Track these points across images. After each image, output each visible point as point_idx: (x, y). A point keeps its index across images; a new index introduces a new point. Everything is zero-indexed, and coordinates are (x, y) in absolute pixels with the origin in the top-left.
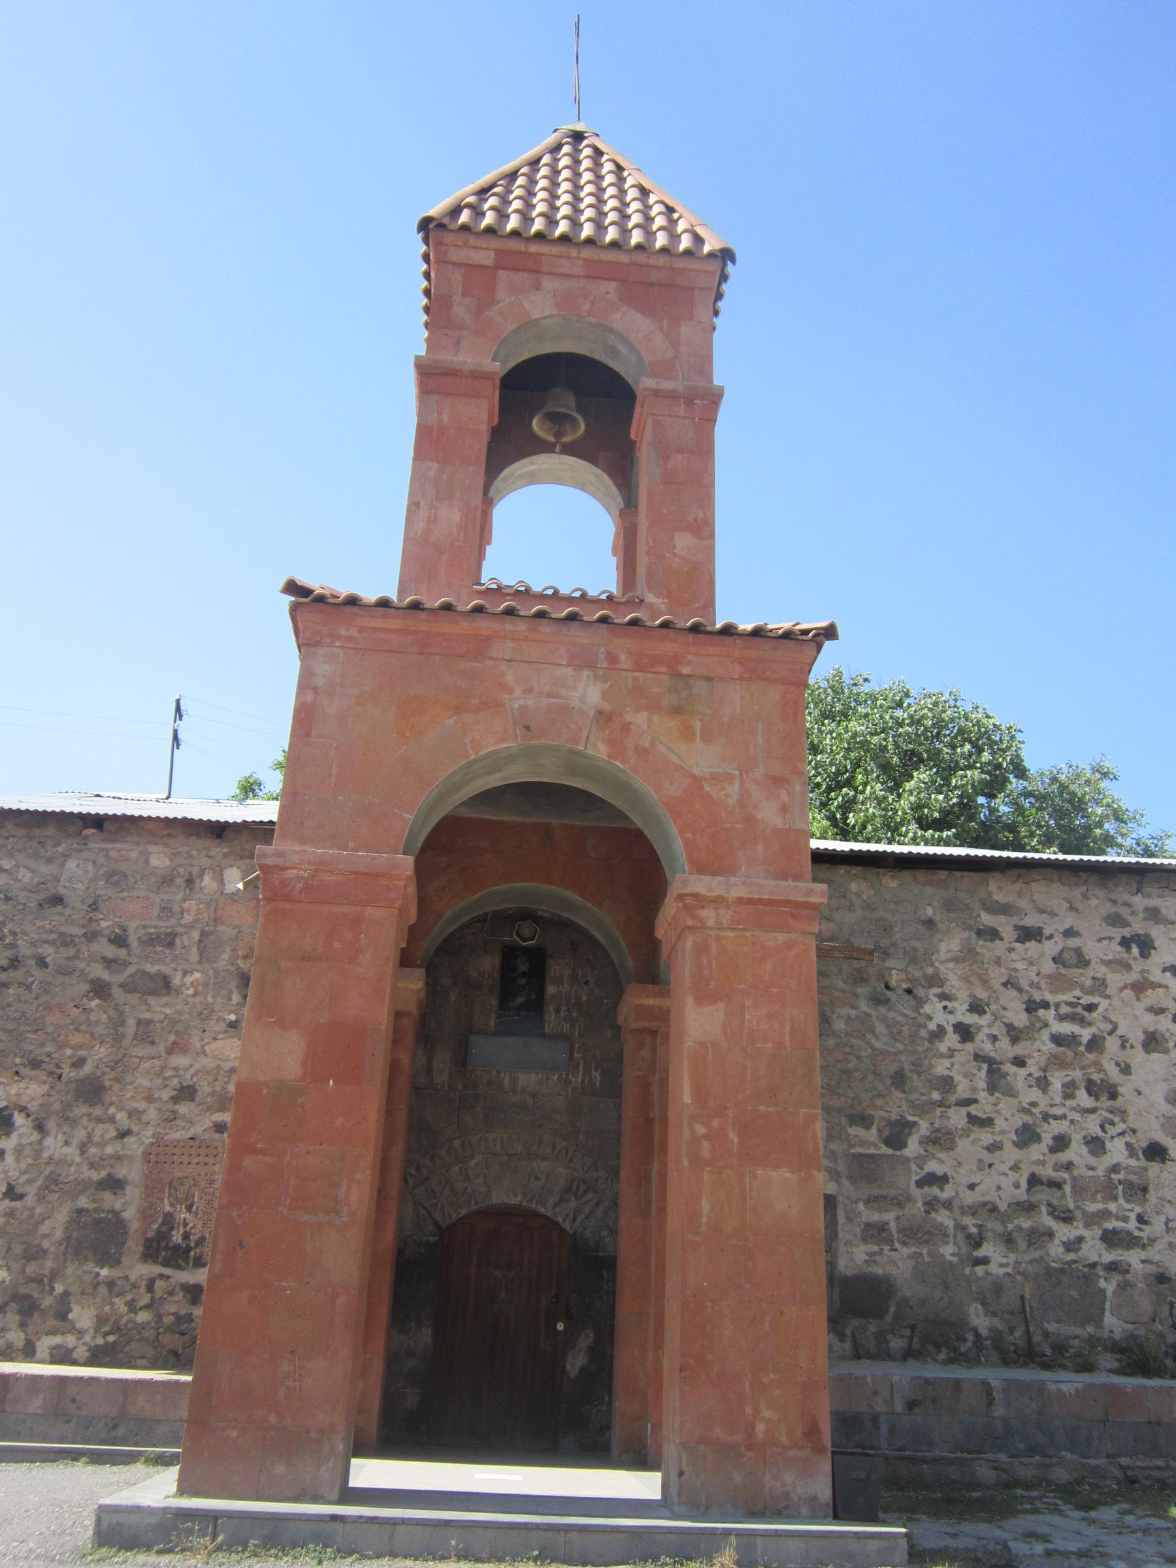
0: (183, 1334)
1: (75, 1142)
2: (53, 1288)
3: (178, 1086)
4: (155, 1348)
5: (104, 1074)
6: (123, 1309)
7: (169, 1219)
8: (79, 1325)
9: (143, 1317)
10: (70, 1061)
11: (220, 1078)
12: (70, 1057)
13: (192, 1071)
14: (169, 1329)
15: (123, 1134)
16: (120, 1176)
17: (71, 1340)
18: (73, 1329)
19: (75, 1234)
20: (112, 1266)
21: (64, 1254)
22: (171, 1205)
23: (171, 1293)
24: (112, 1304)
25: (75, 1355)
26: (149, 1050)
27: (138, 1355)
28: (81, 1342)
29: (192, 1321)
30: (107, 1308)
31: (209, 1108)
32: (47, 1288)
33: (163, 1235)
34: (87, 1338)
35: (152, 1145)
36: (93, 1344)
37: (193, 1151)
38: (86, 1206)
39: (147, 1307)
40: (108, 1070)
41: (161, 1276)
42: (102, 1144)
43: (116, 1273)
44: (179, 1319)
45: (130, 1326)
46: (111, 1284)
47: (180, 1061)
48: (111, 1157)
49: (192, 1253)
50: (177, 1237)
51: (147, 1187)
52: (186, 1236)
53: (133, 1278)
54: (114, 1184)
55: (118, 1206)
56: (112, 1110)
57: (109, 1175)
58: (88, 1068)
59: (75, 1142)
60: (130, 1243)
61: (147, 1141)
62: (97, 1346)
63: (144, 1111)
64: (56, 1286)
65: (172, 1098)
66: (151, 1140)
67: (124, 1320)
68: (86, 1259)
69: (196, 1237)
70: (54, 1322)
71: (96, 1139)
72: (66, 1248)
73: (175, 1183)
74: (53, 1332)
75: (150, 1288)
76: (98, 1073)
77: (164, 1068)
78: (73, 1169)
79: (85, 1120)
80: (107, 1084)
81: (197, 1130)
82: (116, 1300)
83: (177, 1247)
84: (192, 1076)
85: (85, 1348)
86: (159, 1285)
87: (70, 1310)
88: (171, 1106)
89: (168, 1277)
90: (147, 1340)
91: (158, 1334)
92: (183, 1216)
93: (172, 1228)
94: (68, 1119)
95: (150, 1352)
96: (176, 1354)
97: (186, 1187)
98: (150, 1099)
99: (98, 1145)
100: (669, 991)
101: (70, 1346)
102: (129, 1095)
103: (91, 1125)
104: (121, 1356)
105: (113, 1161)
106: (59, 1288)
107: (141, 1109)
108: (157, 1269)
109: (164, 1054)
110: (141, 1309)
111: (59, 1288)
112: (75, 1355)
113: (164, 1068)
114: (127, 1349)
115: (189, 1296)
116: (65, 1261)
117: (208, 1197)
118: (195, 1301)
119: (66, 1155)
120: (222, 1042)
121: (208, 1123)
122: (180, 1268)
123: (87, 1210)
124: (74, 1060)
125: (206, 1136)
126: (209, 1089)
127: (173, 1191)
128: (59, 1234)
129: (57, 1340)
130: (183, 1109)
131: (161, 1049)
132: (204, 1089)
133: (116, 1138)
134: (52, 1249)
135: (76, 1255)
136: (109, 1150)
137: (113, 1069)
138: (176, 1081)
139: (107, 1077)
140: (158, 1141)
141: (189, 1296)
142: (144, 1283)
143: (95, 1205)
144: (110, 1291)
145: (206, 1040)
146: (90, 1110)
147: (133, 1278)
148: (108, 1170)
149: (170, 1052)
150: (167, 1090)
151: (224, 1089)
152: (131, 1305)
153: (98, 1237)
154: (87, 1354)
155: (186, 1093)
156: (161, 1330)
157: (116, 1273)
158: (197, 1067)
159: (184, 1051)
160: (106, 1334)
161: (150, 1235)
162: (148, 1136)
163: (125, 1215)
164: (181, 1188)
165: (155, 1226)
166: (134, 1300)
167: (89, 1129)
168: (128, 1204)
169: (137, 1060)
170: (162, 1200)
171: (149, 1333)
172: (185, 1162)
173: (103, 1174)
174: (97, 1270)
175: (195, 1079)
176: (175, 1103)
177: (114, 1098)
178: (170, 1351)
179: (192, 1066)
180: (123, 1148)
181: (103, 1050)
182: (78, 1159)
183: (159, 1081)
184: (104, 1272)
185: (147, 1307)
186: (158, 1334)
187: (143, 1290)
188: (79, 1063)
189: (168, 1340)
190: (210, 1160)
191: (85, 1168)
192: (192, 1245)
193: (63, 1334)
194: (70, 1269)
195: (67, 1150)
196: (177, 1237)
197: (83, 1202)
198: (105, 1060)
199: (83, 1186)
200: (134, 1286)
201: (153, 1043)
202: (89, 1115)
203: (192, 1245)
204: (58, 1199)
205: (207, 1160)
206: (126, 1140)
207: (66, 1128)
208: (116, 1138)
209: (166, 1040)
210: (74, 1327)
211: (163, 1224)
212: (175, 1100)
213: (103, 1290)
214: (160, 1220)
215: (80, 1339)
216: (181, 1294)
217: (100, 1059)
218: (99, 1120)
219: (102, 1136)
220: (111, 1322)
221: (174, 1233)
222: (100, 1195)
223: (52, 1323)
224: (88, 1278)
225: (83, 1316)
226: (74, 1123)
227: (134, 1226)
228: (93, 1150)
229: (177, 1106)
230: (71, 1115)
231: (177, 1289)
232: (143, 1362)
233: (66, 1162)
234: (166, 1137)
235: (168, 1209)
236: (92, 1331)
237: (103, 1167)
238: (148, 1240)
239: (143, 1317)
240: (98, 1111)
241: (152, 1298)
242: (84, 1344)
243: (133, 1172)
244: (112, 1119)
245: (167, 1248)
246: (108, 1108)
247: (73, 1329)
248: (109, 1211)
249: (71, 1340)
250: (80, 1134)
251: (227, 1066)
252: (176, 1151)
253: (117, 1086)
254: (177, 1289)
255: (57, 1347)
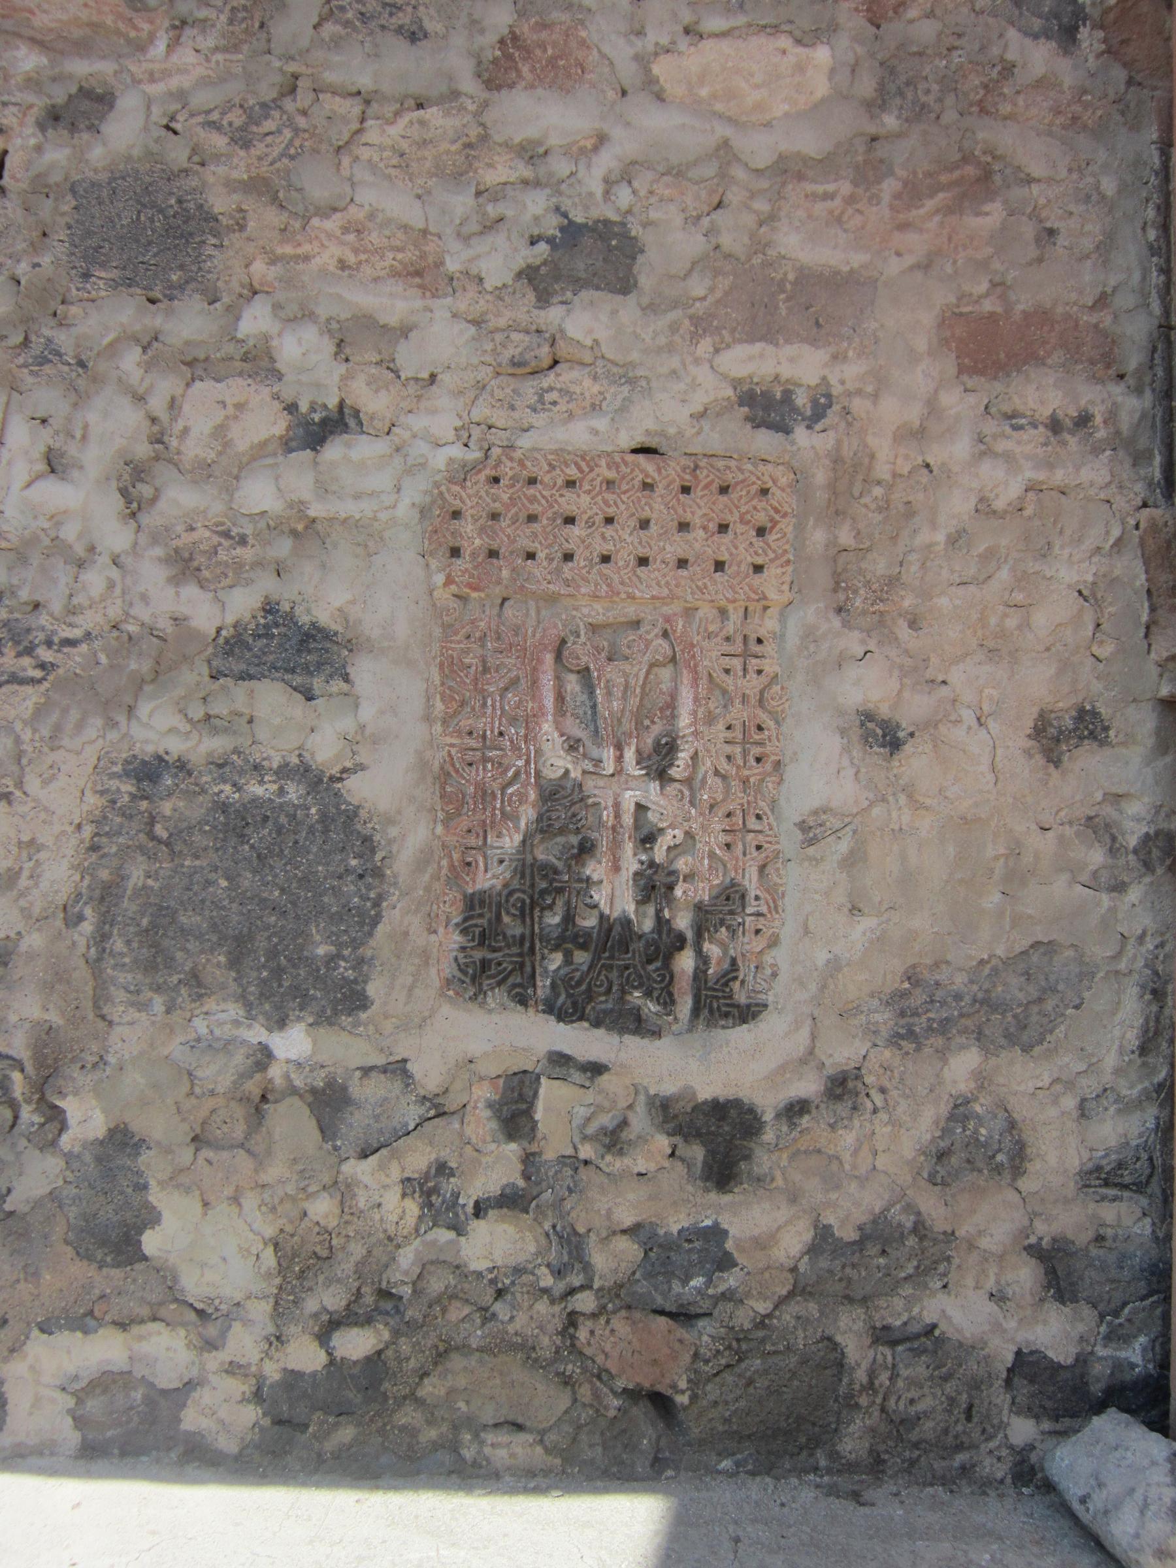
0: (683, 1316)
1: (95, 458)
2: (56, 1117)
3: (551, 225)
4: (566, 1381)
5: (201, 158)
6: (399, 1210)
7: (562, 806)
8: (193, 1285)
9: (493, 1244)
10: (39, 103)
11: (734, 196)
12: (32, 83)
13: (606, 161)
14: (620, 1298)
15: (320, 429)
16: (324, 617)
17: (166, 1351)
18: (170, 1302)
19: (136, 874)
20: (324, 1019)
21: (95, 965)
22: (573, 746)
23: (614, 1139)
24: (343, 1190)
25: (192, 1420)
26: (393, 66)
27: (488, 1415)
28: (213, 1361)
29: (726, 1262)
30: (322, 1208)
31: (701, 326)
32: (29, 1115)
33: (544, 883)
34: (244, 1343)
35: (462, 474)
36: (272, 1372)
37: (657, 508)
38: (175, 747)
39: (511, 1201)
40: (219, 142)
41: (560, 1061)
42: (223, 471)
43: (345, 1050)
44: (661, 1253)
45: (436, 1285)
46: (328, 1101)
47: (540, 114)
48: (275, 527)
49: (685, 962)
50: (613, 892)
51: (450, 667)
52: (654, 885)
53: (429, 1072)
54: (299, 651)
55: (325, 750)
56: (256, 321)
57: (269, 608)
58: (124, 133)
59: (95, 458)
60: (398, 916)
61: (440, 459)
62: (292, 1378)
63: (405, 331)
64: (71, 1106)
65: (529, 274)
66: (456, 451)
67: (407, 1258)
68: (196, 983)
69: (703, 892)
70: (81, 1271)
71: (194, 449)
72: (101, 938)
73: (581, 651)
74: (83, 1321)
75: (515, 1113)
76: (178, 154)
77: (476, 146)
78: (95, 580)
79: (131, 360)
80: (221, 203)
81: (665, 412)
82: (361, 1170)
83: (614, 937)
84: (609, 183)
85: (238, 1387)
86: (554, 1100)
87: (151, 1218)
88: (523, 308)
89: (596, 1069)
90: (526, 1349)
91: (572, 1320)
92: (629, 798)
93: (586, 849)
94: (50, 355)
95: (548, 1402)
96: (660, 1402)
97: (637, 670)
98: (423, 275)
99: (203, 472)
100: (478, 996)
101: (167, 1379)
102: (327, 257)
103: (165, 386)
104: (408, 1416)
105: (283, 548)
106: (86, 1119)
107: (392, 320)
108: (533, 1034)
109: (469, 85)
110: (479, 1210)
111: (86, 1119)
112: (192, 1420)
113: (476, 146)
114: (431, 1389)
115: (697, 1153)
116: (100, 999)
117: (738, 713)
118: (723, 1172)
119: (57, 519)
120: (725, 45)
121: (710, 388)
122: (637, 1024)
123: (182, 766)
124: (59, 95)
125: (712, 438)
126: (692, 244)
127: (572, 684)
128: (58, 875)
129: (104, 1350)
130: (584, 321)
131: (455, 60)
132: (671, 242)
133: (287, 445)
134: (34, 940)
135: (150, 967)
136: (260, 495)
137: (242, 139)
138: (536, 204)
139: (215, 173)
140: (487, 465)
141: (697, 1153)
142: (484, 1093)
143: (216, 744)
144: (327, 1131)
145: (655, 36)
146: (155, 319)
147: (429, 1072)
148: (267, 585)
149: (498, 73)
150: (499, 239)
151: (760, 246)
152: (432, 1192)
153: (248, 892)
154: (251, 1414)
155: (590, 255)
156: (585, 1302)
157: (345, 1050)
158: (624, 145)
159: (562, 71)
160: (328, 1327)
161: (490, 878)
162: (436, 433)
163: (357, 789)
164: (613, 673)
165: (510, 842)
166: (442, 1169)
167: (157, 404)
168: (378, 741)
169: (353, 108)
170: (530, 721)
171: (532, 1319)
172: (624, 557)
173: (242, 604)
174: (257, 1034)
175: (624, 196)
176: (544, 299)
177: (259, 267)
178: (633, 1395)
179: (602, 139)
180: (323, 490)
181: (185, 56)
182: (116, 537)
183: (462, 203)
184: (293, 1044)
185: (511, 1201)
186: (572, 1320)
187: (481, 1124)
188: (79, 112)
189: (617, 1343)
190: (740, 548)
191: (152, 575)
192: (683, 922)
193: (122, 1326)
194: (132, 1033)
195: (57, 494)
196: (613, 892)
197: (158, 728)
198: (201, 99)
199: (157, 655)
200: (438, 1109)
201: (414, 36)
202: (149, 342)
203: (683, 922)
204: (39, 712)
205: (723, 547)
206: (333, 451)
207: (48, 397)
208: (287, 445)
209: (475, 25)
210: (173, 1293)
211: (544, 828)
212: (540, 282)
213: (292, 1124)
214: (528, 814)
215: (211, 1345)
216: (663, 1142)
217: (181, 96)
218: (195, 366)
219: (220, 431)
220: (345, 1267)
221: (594, 869)
222: (237, 697)
223: (67, 1274)
224: (218, 1074)
225: (210, 1241)
226: (83, 372)
227: (413, 843)
228: (180, 499)
229: (553, 315)
230: (64, 340)
231: (639, 1122)
232: (505, 1449)
233: (58, 546)
234: (525, 442)
235: (557, 762)
236: (260, 1310)
237: (239, 573)
238: (474, 903)
239: (493, 1244)
240: (189, 323)
241: (528, 1159)
242: (233, 1369)
243: (380, 595)
244: (259, 362)
245: (570, 938)
246: (234, 312)
247: (170, 1302)
248: (284, 772)
249: (166, 1351)
250: (113, 426)
251: (760, 148)
252: (578, 502)
253: (264, 218)
254: (639, 1122)
255: (106, 1382)
